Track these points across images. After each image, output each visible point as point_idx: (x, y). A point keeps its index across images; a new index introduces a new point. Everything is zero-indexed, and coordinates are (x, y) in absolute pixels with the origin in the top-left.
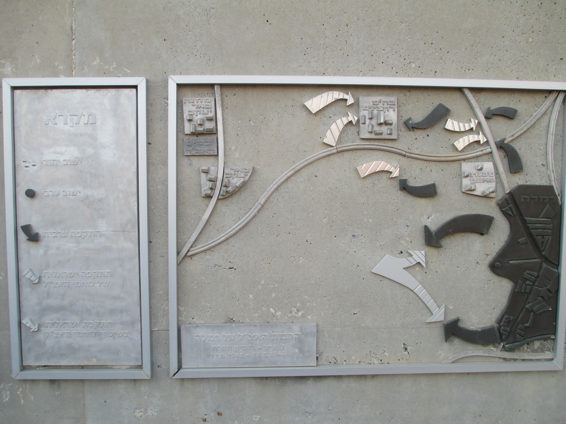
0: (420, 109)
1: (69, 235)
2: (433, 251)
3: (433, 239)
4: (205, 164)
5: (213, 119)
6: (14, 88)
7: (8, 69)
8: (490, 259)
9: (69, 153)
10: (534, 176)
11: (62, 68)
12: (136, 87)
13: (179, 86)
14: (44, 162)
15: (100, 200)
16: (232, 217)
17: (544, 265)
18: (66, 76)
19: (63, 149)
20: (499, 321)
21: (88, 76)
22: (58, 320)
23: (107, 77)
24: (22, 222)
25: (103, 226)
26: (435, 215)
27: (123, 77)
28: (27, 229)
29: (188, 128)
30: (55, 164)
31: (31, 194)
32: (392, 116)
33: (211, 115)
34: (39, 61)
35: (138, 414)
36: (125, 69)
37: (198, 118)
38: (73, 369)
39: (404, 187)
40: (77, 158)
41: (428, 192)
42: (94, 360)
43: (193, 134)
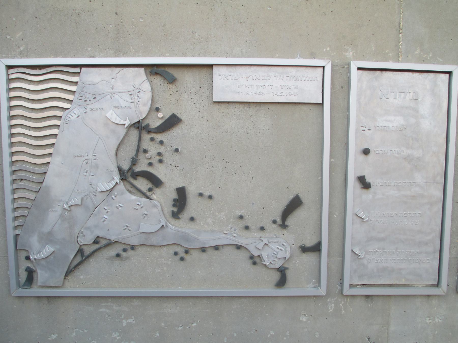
1: (392, 184)
9: (397, 121)
11: (391, 55)
14: (378, 128)
15: (418, 159)
18: (394, 61)
19: (392, 118)
21: (411, 63)
22: (379, 249)
23: (425, 63)
25: (419, 178)
27: (437, 64)
30: (385, 129)
34: (373, 48)
35: (428, 321)
36: (438, 59)
38: (384, 287)
40: (403, 125)
42: (403, 280)
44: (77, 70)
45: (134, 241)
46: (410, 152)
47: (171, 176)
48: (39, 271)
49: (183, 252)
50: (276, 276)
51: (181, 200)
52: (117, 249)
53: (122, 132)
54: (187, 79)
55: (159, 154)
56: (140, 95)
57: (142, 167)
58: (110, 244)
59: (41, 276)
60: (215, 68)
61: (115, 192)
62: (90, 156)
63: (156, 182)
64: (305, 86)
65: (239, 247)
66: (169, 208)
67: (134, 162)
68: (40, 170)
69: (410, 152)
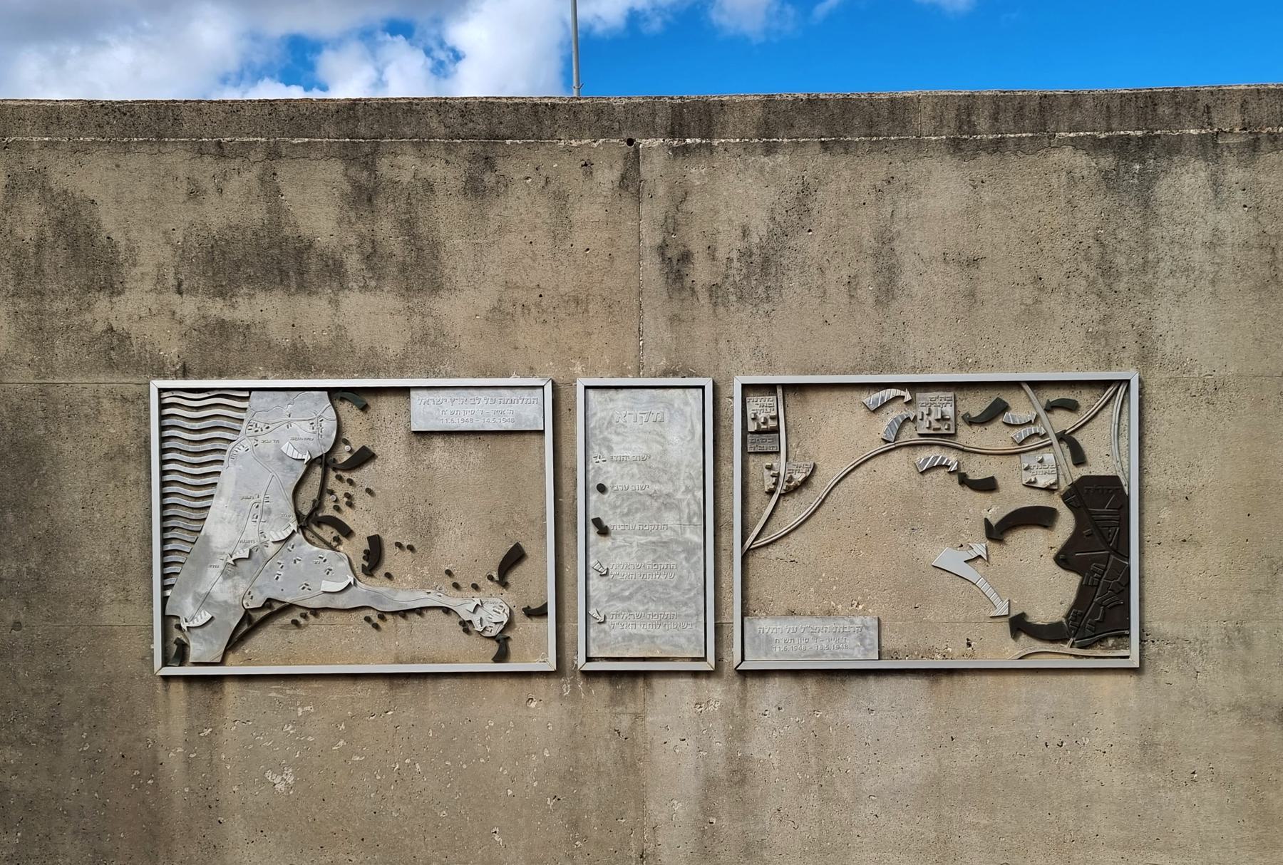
0: (976, 404)
2: (994, 547)
3: (996, 532)
4: (768, 461)
5: (776, 418)
6: (586, 388)
7: (578, 369)
8: (1054, 552)
10: (1098, 467)
12: (703, 388)
13: (744, 386)
16: (793, 511)
17: (1112, 557)
20: (1067, 617)
24: (592, 516)
26: (994, 508)
28: (597, 522)
29: (752, 427)
31: (602, 489)
32: (949, 411)
33: (774, 414)
37: (761, 417)
39: (964, 480)
41: (988, 486)
43: (756, 432)
44: (246, 394)
45: (315, 604)
46: (657, 487)
47: (362, 521)
48: (192, 644)
49: (378, 619)
50: (493, 648)
51: (374, 556)
52: (296, 615)
53: (301, 469)
54: (384, 406)
55: (348, 496)
56: (324, 424)
57: (328, 511)
58: (289, 607)
59: (197, 650)
60: (413, 393)
61: (292, 542)
62: (262, 498)
63: (347, 532)
64: (530, 410)
65: (447, 611)
66: (359, 562)
67: (318, 505)
68: (195, 515)
69: (657, 487)
